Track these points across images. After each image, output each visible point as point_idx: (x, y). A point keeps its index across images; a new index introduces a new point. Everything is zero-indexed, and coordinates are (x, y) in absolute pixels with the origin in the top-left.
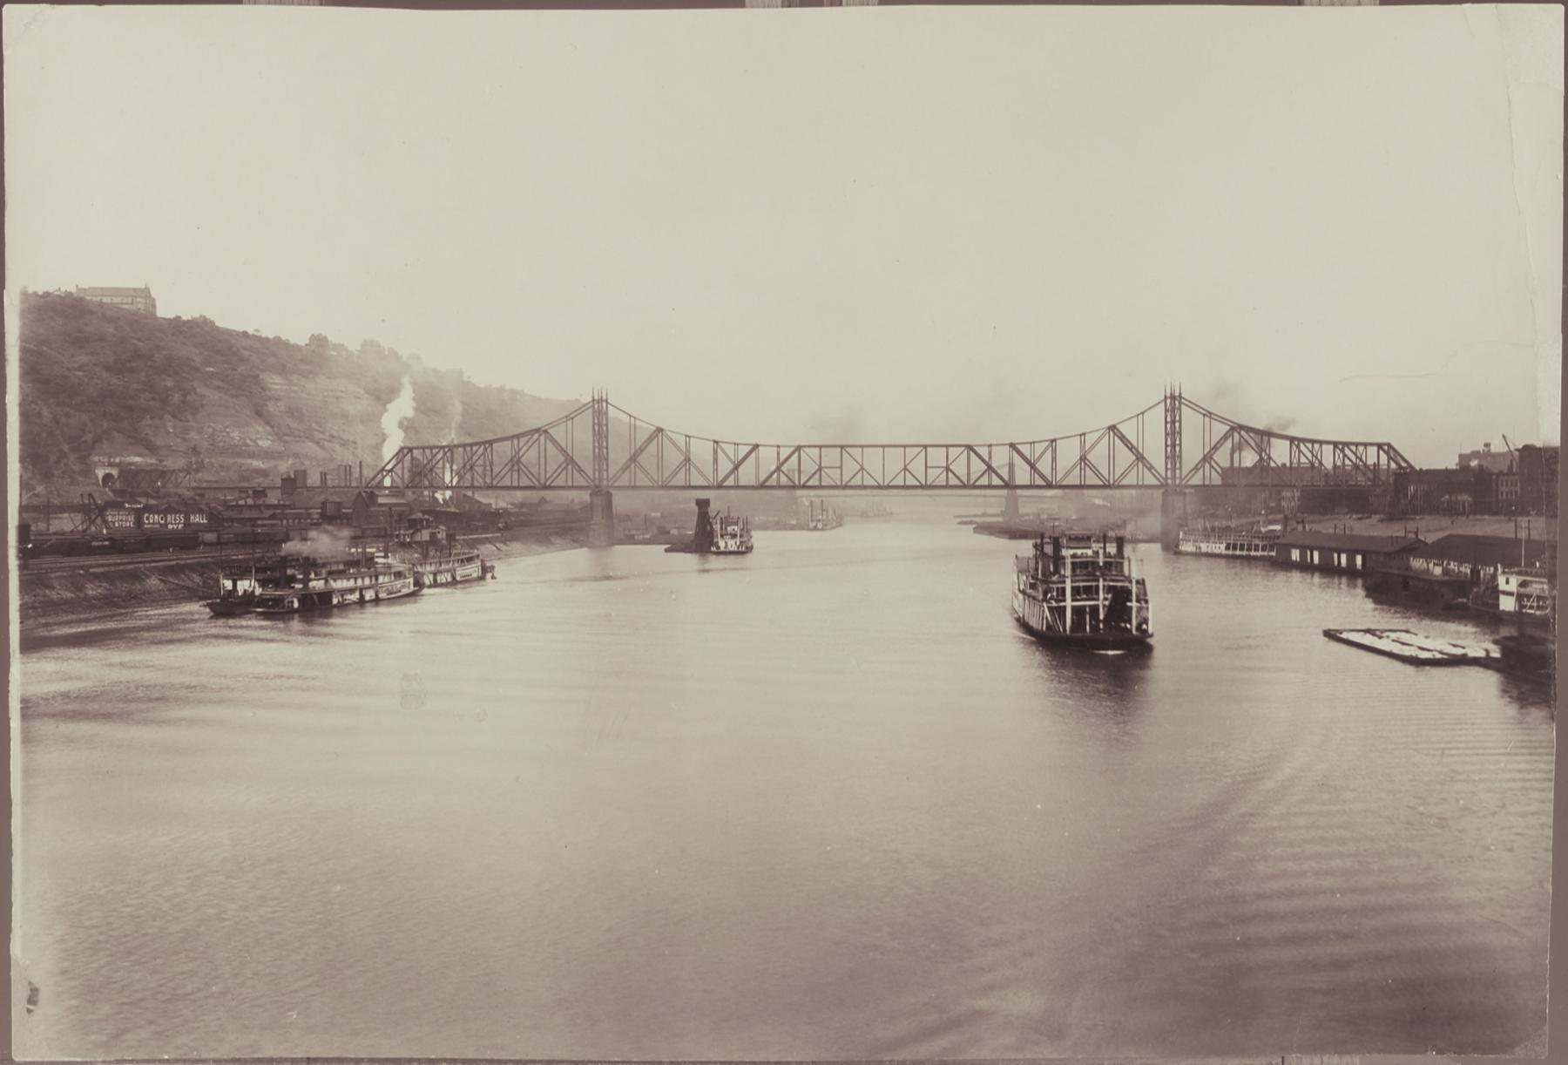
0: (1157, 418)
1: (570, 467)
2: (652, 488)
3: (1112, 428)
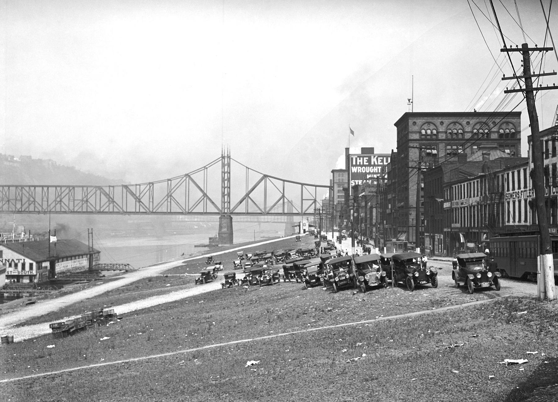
0: (216, 172)
1: (205, 198)
2: (182, 213)
3: (187, 175)
